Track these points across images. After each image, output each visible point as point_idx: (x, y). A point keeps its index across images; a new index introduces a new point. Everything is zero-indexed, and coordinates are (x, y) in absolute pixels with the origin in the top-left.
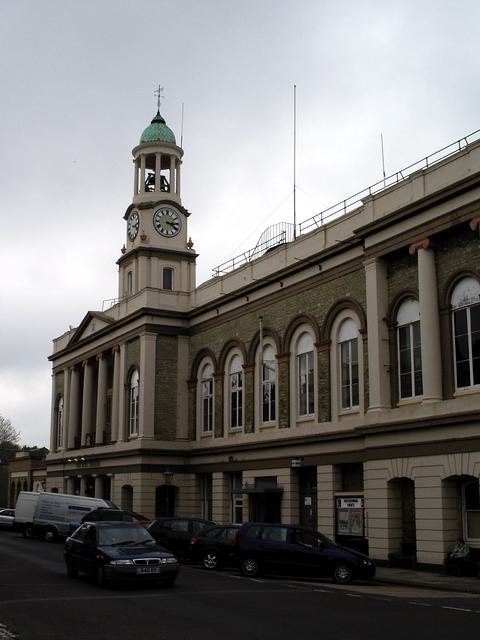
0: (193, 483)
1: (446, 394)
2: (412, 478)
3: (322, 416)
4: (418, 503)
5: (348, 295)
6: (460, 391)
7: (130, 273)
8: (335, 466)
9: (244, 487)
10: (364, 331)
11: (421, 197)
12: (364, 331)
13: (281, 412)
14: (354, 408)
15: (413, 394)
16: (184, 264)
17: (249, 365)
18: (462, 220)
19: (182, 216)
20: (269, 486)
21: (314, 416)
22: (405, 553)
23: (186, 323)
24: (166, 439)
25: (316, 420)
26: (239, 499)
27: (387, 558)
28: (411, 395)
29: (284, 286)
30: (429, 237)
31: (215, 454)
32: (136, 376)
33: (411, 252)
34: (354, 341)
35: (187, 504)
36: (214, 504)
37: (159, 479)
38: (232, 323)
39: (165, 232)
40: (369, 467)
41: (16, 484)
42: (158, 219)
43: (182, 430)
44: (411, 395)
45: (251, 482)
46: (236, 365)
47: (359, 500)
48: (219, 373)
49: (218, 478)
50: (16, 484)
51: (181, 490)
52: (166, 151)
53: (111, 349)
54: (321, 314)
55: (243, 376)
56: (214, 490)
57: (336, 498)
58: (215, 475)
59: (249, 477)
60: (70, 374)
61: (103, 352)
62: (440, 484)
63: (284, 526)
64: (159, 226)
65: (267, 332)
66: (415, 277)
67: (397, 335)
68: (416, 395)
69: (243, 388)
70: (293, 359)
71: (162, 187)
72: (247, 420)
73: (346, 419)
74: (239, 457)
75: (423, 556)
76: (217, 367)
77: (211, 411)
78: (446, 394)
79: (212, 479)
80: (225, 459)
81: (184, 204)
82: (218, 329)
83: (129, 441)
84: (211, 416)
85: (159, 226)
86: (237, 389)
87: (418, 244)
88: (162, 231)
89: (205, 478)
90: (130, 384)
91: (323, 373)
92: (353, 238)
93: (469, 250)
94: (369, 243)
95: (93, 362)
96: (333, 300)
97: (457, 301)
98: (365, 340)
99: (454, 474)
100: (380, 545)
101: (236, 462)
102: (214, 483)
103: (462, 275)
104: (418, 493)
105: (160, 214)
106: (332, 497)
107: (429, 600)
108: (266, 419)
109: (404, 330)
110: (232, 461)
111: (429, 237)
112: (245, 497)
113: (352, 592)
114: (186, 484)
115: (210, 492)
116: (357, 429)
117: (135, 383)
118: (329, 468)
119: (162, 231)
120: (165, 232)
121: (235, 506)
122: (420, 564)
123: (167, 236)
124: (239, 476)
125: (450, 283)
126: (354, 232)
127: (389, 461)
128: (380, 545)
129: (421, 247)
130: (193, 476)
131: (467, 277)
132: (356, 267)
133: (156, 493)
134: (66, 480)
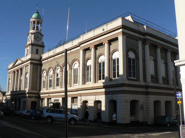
1: (84, 83)
2: (161, 101)
7: (28, 50)
10: (79, 67)
11: (71, 47)
12: (79, 67)
13: (60, 84)
14: (76, 84)
15: (116, 77)
16: (42, 48)
17: (54, 73)
18: (101, 42)
19: (41, 36)
24: (34, 90)
27: (93, 120)
28: (101, 80)
30: (108, 41)
38: (51, 63)
40: (79, 98)
44: (101, 80)
46: (51, 73)
48: (47, 74)
53: (22, 68)
57: (71, 105)
59: (53, 100)
60: (12, 74)
63: (114, 117)
64: (36, 38)
65: (58, 65)
66: (91, 55)
67: (86, 68)
68: (102, 79)
69: (52, 79)
70: (73, 70)
74: (51, 95)
76: (47, 73)
77: (59, 81)
78: (84, 83)
80: (47, 95)
81: (42, 34)
82: (48, 64)
84: (59, 82)
85: (36, 38)
86: (51, 79)
90: (26, 77)
94: (81, 46)
95: (18, 71)
96: (73, 59)
97: (99, 61)
104: (117, 103)
109: (114, 60)
111: (108, 41)
116: (76, 89)
117: (27, 77)
118: (70, 98)
123: (38, 41)
125: (113, 51)
126: (78, 43)
127: (131, 95)
131: (116, 51)
132: (78, 52)
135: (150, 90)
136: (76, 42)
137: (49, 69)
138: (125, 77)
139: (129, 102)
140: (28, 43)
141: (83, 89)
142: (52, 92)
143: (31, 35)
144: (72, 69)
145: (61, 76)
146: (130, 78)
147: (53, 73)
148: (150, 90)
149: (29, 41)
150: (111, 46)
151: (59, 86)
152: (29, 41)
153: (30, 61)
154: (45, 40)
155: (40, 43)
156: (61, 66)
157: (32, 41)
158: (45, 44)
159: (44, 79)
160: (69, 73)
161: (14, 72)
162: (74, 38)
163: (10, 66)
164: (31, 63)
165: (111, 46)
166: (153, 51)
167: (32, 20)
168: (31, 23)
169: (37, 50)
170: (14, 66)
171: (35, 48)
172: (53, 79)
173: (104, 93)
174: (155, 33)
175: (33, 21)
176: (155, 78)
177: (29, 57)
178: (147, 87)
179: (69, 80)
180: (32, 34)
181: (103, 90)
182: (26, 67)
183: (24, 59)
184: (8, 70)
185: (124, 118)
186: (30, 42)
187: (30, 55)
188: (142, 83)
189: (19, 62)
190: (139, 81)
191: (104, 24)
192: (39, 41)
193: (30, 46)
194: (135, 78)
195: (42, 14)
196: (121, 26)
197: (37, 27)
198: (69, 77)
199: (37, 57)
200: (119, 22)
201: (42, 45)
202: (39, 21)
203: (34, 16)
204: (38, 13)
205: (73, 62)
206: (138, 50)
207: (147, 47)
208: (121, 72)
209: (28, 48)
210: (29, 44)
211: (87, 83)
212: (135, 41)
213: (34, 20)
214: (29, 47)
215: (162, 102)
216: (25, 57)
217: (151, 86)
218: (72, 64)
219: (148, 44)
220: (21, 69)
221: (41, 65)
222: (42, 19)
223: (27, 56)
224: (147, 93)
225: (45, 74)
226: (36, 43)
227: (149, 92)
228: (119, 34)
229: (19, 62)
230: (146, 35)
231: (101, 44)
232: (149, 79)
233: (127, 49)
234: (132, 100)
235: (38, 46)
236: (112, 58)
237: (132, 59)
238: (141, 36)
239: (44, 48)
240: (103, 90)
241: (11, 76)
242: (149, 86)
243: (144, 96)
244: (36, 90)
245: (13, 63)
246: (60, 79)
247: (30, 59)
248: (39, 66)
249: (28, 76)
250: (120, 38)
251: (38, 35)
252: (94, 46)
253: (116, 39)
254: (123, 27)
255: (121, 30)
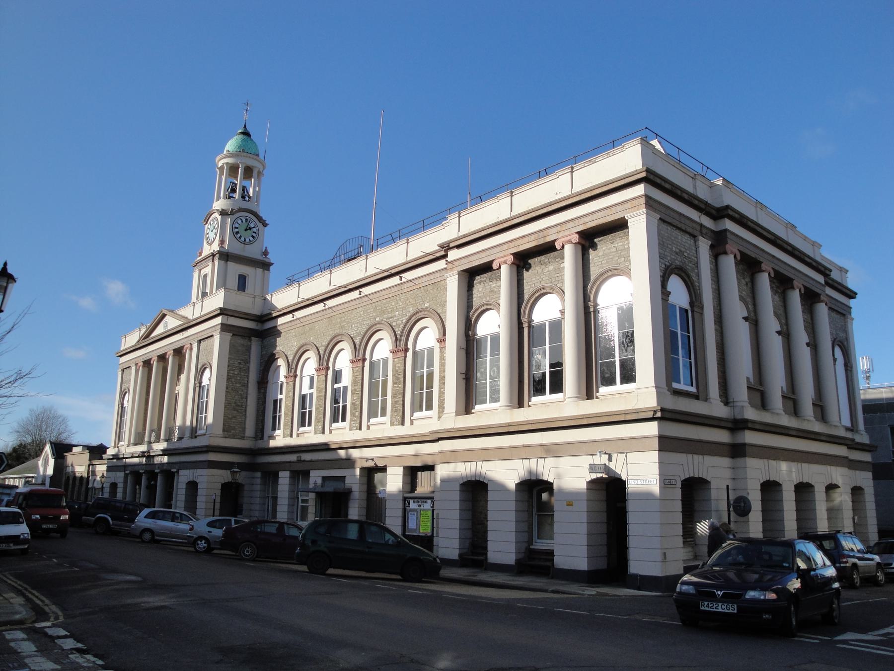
0: (259, 481)
3: (394, 420)
4: (490, 506)
5: (427, 305)
6: (603, 390)
7: (205, 276)
8: (292, 472)
9: (311, 486)
10: (442, 340)
12: (442, 340)
13: (353, 414)
16: (259, 271)
18: (549, 239)
20: (338, 486)
21: (387, 419)
22: (475, 551)
23: (260, 324)
24: (233, 437)
25: (313, 432)
26: (305, 498)
29: (404, 280)
31: (284, 453)
32: (207, 373)
33: (495, 266)
34: (431, 351)
35: (253, 506)
36: (279, 501)
37: (224, 476)
39: (243, 239)
41: (71, 479)
42: (237, 225)
43: (250, 430)
45: (320, 481)
47: (429, 501)
49: (284, 477)
50: (71, 479)
51: (246, 488)
52: (251, 162)
53: (182, 347)
54: (399, 322)
55: (316, 378)
56: (280, 488)
58: (281, 474)
59: (316, 477)
61: (174, 350)
62: (458, 488)
64: (237, 233)
67: (470, 347)
69: (314, 391)
71: (243, 197)
72: (317, 422)
73: (425, 422)
74: (307, 457)
75: (494, 556)
78: (589, 394)
79: (278, 477)
80: (293, 458)
83: (196, 437)
85: (237, 233)
87: (502, 260)
88: (240, 237)
89: (270, 475)
90: (200, 383)
91: (398, 379)
92: (436, 252)
93: (551, 268)
94: (453, 255)
95: (162, 358)
96: (412, 310)
98: (442, 350)
99: (692, 475)
100: (449, 545)
101: (304, 461)
102: (280, 481)
103: (610, 274)
105: (240, 222)
106: (401, 498)
107: (527, 601)
108: (303, 425)
110: (300, 461)
111: (578, 233)
112: (312, 496)
113: (449, 593)
114: (254, 483)
115: (275, 490)
116: (432, 433)
117: (205, 381)
118: (400, 470)
119: (240, 237)
120: (243, 239)
121: (300, 504)
122: (635, 576)
123: (245, 243)
124: (306, 474)
128: (449, 545)
129: (505, 262)
130: (259, 474)
133: (222, 489)
134: (126, 476)
135: (722, 436)
136: (426, 242)
137: (301, 353)
138: (219, 431)
139: (679, 485)
140: (207, 250)
141: (585, 422)
142: (391, 438)
143: (219, 218)
144: (364, 360)
145: (354, 382)
146: (675, 385)
147: (318, 370)
148: (750, 437)
149: (210, 244)
150: (592, 254)
151: (344, 420)
152: (210, 244)
153: (219, 320)
154: (271, 240)
155: (253, 251)
156: (357, 341)
157: (222, 242)
158: (271, 258)
159: (306, 382)
160: (394, 366)
161: (147, 363)
162: (426, 222)
163: (132, 339)
164: (225, 328)
165: (526, 274)
166: (743, 282)
167: (222, 162)
168: (221, 174)
169: (242, 279)
170: (147, 340)
171: (236, 269)
172: (319, 391)
173: (656, 442)
174: (750, 212)
175: (227, 164)
176: (759, 393)
177: (217, 301)
178: (738, 425)
179: (394, 396)
180: (223, 213)
181: (652, 429)
182: (123, 370)
183: (191, 312)
184: (121, 356)
185: (665, 554)
186: (216, 247)
187: (221, 294)
188: (716, 408)
189: (171, 323)
190: (706, 399)
191: (450, 211)
192: (251, 243)
193: (216, 262)
194: (693, 389)
195: (262, 138)
196: (644, 175)
197: (244, 189)
198: (394, 383)
199: (246, 303)
200: (628, 159)
201: (261, 258)
202: (247, 168)
203: (231, 145)
204: (246, 133)
205: (409, 326)
206: (698, 275)
207: (729, 263)
208: (210, 420)
209: (207, 270)
210: (213, 255)
211: (478, 408)
212: (686, 239)
213: (230, 160)
214: (210, 264)
215: (713, 485)
216: (198, 306)
217: (753, 422)
218: (405, 334)
219: (732, 253)
220: (179, 352)
221: (274, 333)
222: (261, 157)
223: (207, 301)
224: (737, 451)
225: (283, 371)
226: (238, 249)
227: (744, 445)
228: (635, 202)
229: (171, 323)
230: (723, 217)
231: (548, 249)
232: (740, 393)
233: (669, 268)
234: (687, 476)
235: (245, 262)
236: (530, 321)
237: (680, 308)
238: (707, 222)
239: (269, 270)
240: (652, 429)
241: (134, 379)
242: (746, 421)
243: (725, 462)
244: (243, 438)
245: (143, 330)
246: (353, 394)
247: (223, 312)
248: (255, 345)
249: (210, 379)
250: (639, 227)
251: (246, 219)
252: (515, 255)
253: (620, 226)
254: (650, 178)
255: (640, 190)
